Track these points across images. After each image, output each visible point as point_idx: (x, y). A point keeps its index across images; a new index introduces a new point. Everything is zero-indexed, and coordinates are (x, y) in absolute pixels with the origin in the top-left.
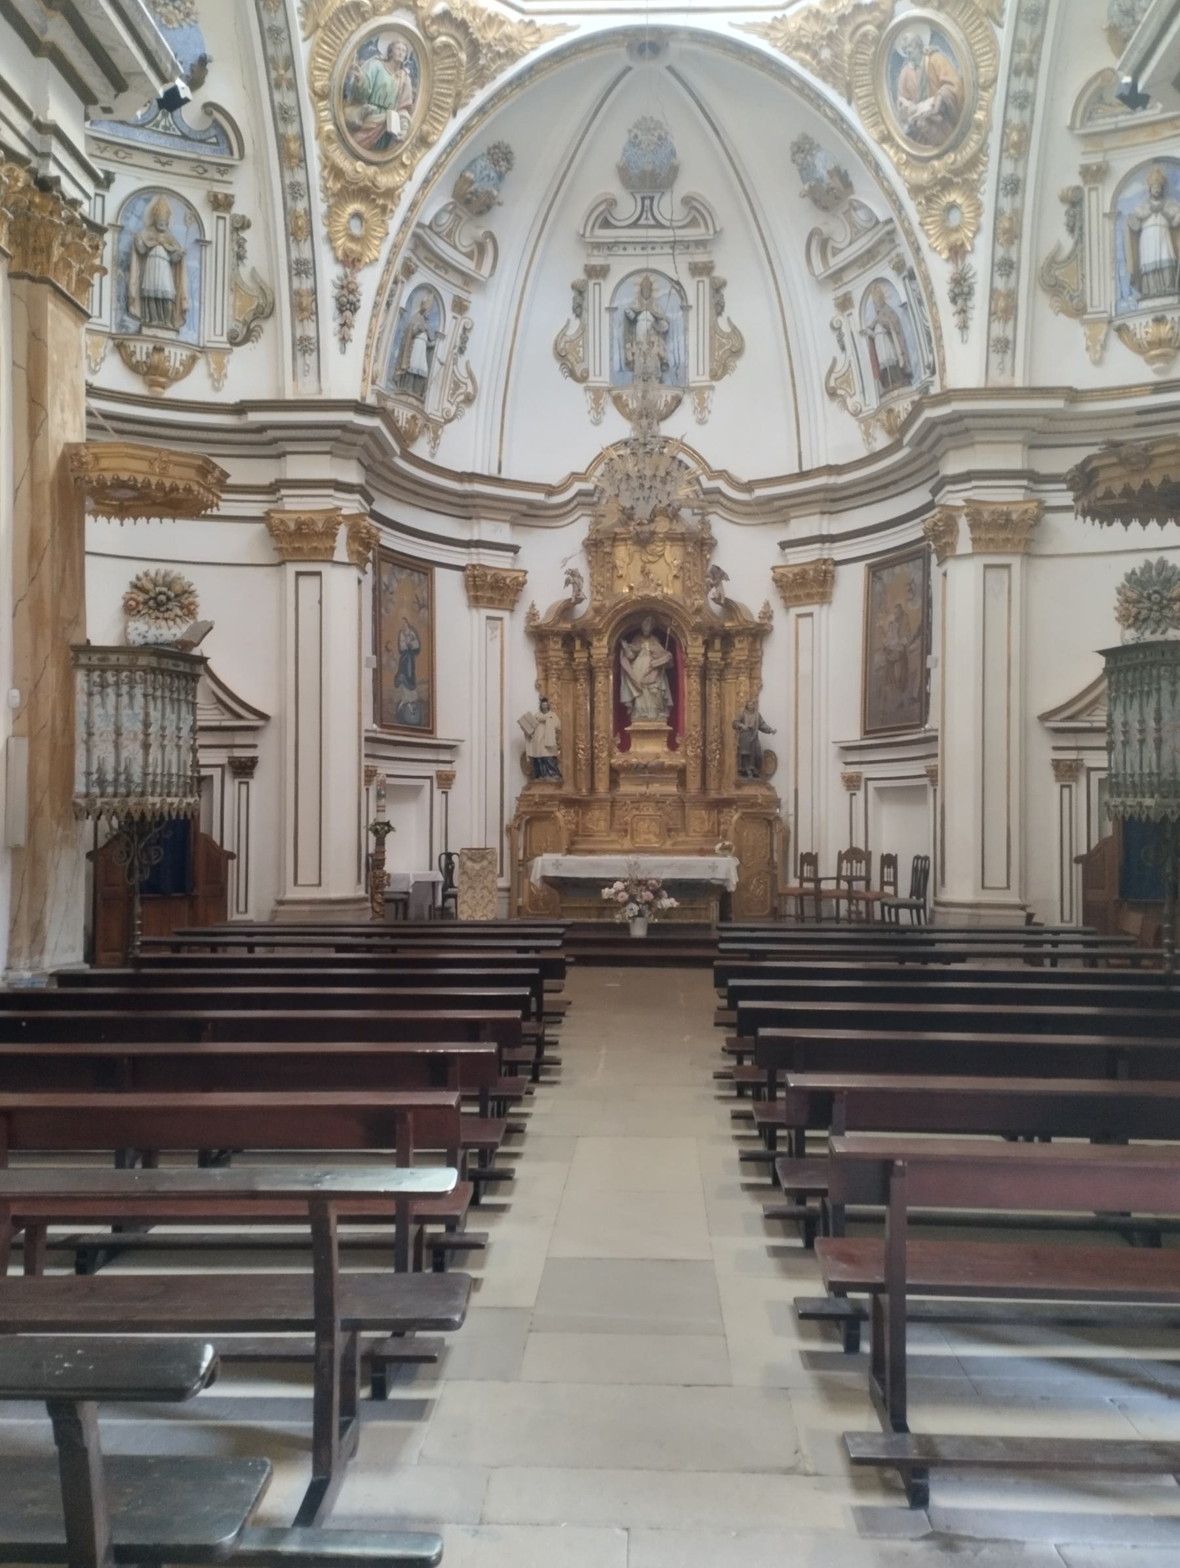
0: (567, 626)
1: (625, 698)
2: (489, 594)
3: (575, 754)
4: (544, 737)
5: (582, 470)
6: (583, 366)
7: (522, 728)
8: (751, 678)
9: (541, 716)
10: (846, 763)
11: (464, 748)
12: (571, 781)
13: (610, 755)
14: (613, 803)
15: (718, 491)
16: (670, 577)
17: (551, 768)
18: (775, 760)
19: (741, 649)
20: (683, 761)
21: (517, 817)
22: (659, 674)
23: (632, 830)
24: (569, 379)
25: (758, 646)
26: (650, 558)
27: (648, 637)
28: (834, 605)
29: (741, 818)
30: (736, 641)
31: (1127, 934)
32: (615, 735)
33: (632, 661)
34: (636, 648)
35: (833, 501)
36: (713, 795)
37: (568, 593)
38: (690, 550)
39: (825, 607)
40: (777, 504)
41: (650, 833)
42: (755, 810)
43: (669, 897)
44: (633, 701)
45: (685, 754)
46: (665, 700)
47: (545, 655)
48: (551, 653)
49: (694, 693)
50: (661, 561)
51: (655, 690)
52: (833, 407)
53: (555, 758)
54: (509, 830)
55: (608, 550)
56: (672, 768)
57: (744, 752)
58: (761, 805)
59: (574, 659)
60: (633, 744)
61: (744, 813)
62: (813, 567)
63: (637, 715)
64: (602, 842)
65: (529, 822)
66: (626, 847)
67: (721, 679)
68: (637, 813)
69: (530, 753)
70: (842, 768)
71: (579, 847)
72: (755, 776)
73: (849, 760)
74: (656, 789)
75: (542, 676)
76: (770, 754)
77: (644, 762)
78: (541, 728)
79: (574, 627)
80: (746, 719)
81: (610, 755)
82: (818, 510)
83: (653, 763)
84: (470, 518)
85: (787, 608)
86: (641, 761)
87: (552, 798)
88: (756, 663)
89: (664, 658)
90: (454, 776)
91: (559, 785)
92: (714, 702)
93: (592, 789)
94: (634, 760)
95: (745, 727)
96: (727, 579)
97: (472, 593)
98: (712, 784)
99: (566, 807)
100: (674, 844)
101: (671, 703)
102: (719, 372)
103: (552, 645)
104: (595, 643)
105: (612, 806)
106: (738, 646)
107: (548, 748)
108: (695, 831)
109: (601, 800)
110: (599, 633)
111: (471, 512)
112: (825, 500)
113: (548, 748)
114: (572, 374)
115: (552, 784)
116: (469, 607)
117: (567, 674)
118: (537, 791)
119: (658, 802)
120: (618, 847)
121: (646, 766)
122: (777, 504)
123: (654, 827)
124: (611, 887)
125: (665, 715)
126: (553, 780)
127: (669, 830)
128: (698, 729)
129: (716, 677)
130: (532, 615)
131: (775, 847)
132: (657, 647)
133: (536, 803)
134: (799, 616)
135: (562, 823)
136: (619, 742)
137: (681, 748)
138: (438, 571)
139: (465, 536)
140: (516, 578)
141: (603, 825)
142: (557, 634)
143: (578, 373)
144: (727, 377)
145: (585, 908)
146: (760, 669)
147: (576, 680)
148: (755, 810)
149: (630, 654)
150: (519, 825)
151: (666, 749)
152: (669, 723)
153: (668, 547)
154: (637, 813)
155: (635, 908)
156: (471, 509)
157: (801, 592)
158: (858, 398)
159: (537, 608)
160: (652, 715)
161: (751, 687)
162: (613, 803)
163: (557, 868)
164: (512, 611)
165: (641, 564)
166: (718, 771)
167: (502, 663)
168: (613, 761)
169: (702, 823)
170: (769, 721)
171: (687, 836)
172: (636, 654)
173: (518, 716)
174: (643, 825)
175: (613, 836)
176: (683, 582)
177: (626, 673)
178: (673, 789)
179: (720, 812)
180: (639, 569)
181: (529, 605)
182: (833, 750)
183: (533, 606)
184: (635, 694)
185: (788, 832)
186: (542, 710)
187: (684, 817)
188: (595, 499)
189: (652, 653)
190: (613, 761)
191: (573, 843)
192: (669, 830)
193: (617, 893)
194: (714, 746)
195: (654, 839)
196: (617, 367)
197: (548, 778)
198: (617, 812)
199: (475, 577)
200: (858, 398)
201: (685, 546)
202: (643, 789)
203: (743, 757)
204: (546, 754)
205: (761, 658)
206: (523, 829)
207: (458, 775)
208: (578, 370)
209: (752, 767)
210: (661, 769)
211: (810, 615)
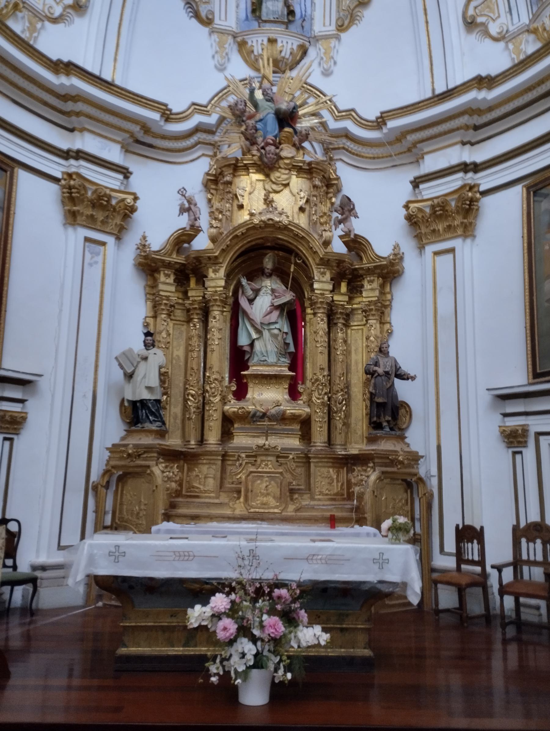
0: (181, 259)
1: (243, 341)
2: (89, 212)
3: (186, 400)
4: (144, 377)
5: (204, 102)
6: (209, 7)
7: (122, 367)
8: (382, 323)
9: (145, 352)
10: (506, 415)
11: (43, 384)
12: (179, 433)
13: (224, 400)
14: (225, 456)
15: (347, 135)
16: (296, 209)
17: (153, 414)
18: (409, 412)
19: (372, 289)
20: (308, 410)
21: (106, 472)
22: (281, 315)
23: (247, 491)
24: (194, 20)
25: (388, 289)
26: (275, 187)
27: (270, 276)
28: (478, 239)
29: (379, 478)
30: (366, 283)
31: (268, 477)
32: (230, 382)
33: (251, 301)
34: (257, 286)
35: (476, 128)
36: (341, 452)
37: (184, 221)
38: (317, 182)
39: (469, 241)
40: (411, 138)
41: (268, 494)
42: (394, 469)
43: (311, 624)
44: (252, 345)
45: (309, 403)
46: (287, 345)
47: (154, 291)
48: (161, 287)
49: (321, 333)
50: (286, 191)
51: (276, 332)
52: (474, 38)
53: (158, 401)
54: (95, 488)
55: (228, 178)
56: (294, 418)
57: (380, 400)
58: (401, 463)
59: (188, 298)
60: (250, 391)
61: (383, 473)
62: (456, 196)
63: (256, 359)
64: (209, 505)
65: (121, 479)
66: (238, 512)
67: (347, 325)
68: (253, 469)
69: (129, 396)
70: (497, 419)
71: (182, 511)
72: (392, 429)
73: (509, 410)
74: (274, 441)
75: (151, 314)
76: (405, 405)
77: (262, 409)
78: (143, 364)
79: (187, 258)
80: (381, 363)
81: (224, 400)
82: (458, 139)
83: (273, 411)
84: (72, 130)
85: (421, 248)
86: (259, 408)
87: (148, 449)
88: (386, 307)
89: (288, 296)
90: (24, 419)
91: (162, 434)
92: (340, 347)
93: (202, 441)
94: (251, 408)
95: (380, 370)
96: (356, 216)
97: (67, 208)
98: (338, 439)
99: (167, 460)
100: (297, 510)
101: (292, 349)
102: (346, 23)
103: (162, 278)
104: (211, 274)
105: (223, 461)
106: (367, 286)
107: (149, 389)
108: (321, 493)
109: (211, 453)
110: (214, 261)
111: (74, 121)
112: (467, 127)
113: (149, 389)
114: (197, 15)
115: (150, 432)
116: (64, 225)
117: (179, 314)
118: (134, 440)
119: (278, 457)
120: (228, 512)
121: (264, 415)
122: (411, 138)
123: (274, 489)
124: (205, 603)
125: (286, 361)
126: (153, 427)
127: (292, 492)
128: (326, 373)
129: (341, 321)
130: (143, 246)
131: (417, 516)
132: (279, 286)
133: (129, 455)
134: (436, 253)
135: (159, 481)
136: (234, 388)
137: (304, 397)
138: (22, 175)
139: (64, 145)
140: (123, 200)
141: (211, 483)
142: (169, 265)
143: (203, 14)
144: (353, 28)
145: (164, 629)
146: (389, 315)
147: (189, 320)
148: (394, 469)
149: (250, 293)
150: (108, 482)
151: (287, 397)
152: (290, 369)
153: (294, 177)
154: (253, 469)
155: (249, 648)
156: (74, 118)
157: (440, 227)
158: (504, 19)
159: (150, 240)
160: (272, 359)
161: (381, 332)
162: (225, 456)
163: (117, 561)
164: (118, 238)
165: (263, 193)
166: (344, 424)
167: (102, 293)
168: (227, 408)
169: (330, 484)
170: (406, 367)
171: (312, 498)
172: (257, 292)
173: (117, 352)
174: (261, 485)
175: (224, 498)
176: (309, 216)
177: (245, 313)
178: (294, 442)
179: (350, 470)
180: (262, 196)
181: (140, 237)
182: (486, 398)
183: (144, 238)
184: (254, 336)
185: (432, 495)
186: (147, 346)
187: (308, 476)
188: (216, 138)
189: (273, 291)
190: (227, 408)
191: (173, 506)
192: (292, 492)
193: (217, 616)
194: (340, 396)
195: (272, 502)
196: (243, 15)
197: (148, 426)
198: (229, 468)
199: (70, 188)
200: (504, 19)
201: (310, 179)
202: (261, 441)
203: (379, 405)
204: (146, 395)
205: (391, 301)
206: (113, 487)
207: (31, 418)
208: (203, 11)
209: (389, 418)
210: (282, 418)
211: (452, 250)
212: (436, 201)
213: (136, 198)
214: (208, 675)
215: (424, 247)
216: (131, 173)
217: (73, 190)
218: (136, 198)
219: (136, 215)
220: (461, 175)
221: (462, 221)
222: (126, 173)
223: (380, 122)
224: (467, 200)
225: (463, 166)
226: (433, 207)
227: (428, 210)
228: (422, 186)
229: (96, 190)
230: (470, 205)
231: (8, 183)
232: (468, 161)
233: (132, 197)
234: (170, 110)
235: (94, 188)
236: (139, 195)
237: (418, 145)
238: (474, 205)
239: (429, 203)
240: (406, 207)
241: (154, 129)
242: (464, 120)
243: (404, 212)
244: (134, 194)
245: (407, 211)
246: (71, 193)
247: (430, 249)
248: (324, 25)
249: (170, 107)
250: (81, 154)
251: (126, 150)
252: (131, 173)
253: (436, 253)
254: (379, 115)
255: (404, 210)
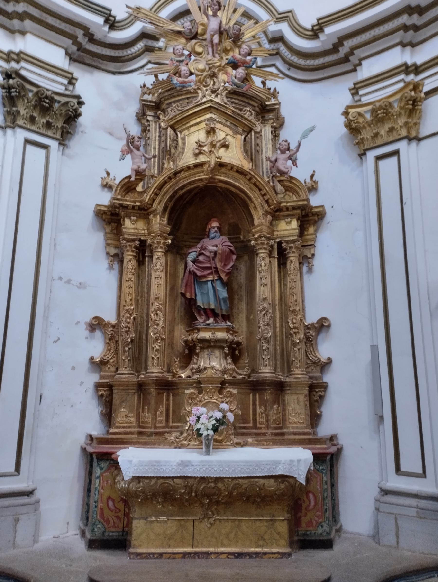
134: (379, 158)
140: (67, 103)
211: (396, 153)
212: (378, 104)
213: (81, 103)
214: (178, 498)
215: (364, 154)
216: (76, 79)
217: (13, 90)
218: (81, 103)
219: (80, 120)
220: (402, 76)
221: (406, 120)
222: (72, 81)
223: (317, 30)
224: (410, 100)
225: (404, 68)
226: (373, 111)
227: (368, 116)
228: (361, 92)
229: (37, 93)
230: (413, 105)
231: (285, 345)
232: (410, 63)
233: (75, 101)
234: (115, 17)
235: (35, 90)
236: (83, 99)
237: (355, 52)
238: (417, 105)
239: (370, 107)
240: (346, 113)
241: (98, 36)
242: (404, 19)
243: (343, 119)
244: (79, 97)
245: (346, 118)
246: (10, 93)
247: (371, 155)
248: (202, 449)
249: (113, 13)
250: (22, 55)
251: (73, 59)
252: (76, 79)
253: (379, 158)
254: (315, 22)
255: (343, 117)
